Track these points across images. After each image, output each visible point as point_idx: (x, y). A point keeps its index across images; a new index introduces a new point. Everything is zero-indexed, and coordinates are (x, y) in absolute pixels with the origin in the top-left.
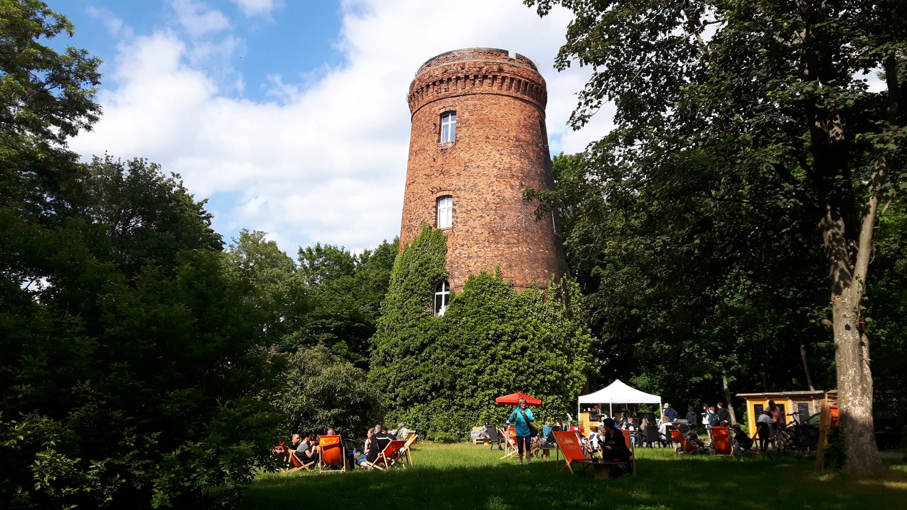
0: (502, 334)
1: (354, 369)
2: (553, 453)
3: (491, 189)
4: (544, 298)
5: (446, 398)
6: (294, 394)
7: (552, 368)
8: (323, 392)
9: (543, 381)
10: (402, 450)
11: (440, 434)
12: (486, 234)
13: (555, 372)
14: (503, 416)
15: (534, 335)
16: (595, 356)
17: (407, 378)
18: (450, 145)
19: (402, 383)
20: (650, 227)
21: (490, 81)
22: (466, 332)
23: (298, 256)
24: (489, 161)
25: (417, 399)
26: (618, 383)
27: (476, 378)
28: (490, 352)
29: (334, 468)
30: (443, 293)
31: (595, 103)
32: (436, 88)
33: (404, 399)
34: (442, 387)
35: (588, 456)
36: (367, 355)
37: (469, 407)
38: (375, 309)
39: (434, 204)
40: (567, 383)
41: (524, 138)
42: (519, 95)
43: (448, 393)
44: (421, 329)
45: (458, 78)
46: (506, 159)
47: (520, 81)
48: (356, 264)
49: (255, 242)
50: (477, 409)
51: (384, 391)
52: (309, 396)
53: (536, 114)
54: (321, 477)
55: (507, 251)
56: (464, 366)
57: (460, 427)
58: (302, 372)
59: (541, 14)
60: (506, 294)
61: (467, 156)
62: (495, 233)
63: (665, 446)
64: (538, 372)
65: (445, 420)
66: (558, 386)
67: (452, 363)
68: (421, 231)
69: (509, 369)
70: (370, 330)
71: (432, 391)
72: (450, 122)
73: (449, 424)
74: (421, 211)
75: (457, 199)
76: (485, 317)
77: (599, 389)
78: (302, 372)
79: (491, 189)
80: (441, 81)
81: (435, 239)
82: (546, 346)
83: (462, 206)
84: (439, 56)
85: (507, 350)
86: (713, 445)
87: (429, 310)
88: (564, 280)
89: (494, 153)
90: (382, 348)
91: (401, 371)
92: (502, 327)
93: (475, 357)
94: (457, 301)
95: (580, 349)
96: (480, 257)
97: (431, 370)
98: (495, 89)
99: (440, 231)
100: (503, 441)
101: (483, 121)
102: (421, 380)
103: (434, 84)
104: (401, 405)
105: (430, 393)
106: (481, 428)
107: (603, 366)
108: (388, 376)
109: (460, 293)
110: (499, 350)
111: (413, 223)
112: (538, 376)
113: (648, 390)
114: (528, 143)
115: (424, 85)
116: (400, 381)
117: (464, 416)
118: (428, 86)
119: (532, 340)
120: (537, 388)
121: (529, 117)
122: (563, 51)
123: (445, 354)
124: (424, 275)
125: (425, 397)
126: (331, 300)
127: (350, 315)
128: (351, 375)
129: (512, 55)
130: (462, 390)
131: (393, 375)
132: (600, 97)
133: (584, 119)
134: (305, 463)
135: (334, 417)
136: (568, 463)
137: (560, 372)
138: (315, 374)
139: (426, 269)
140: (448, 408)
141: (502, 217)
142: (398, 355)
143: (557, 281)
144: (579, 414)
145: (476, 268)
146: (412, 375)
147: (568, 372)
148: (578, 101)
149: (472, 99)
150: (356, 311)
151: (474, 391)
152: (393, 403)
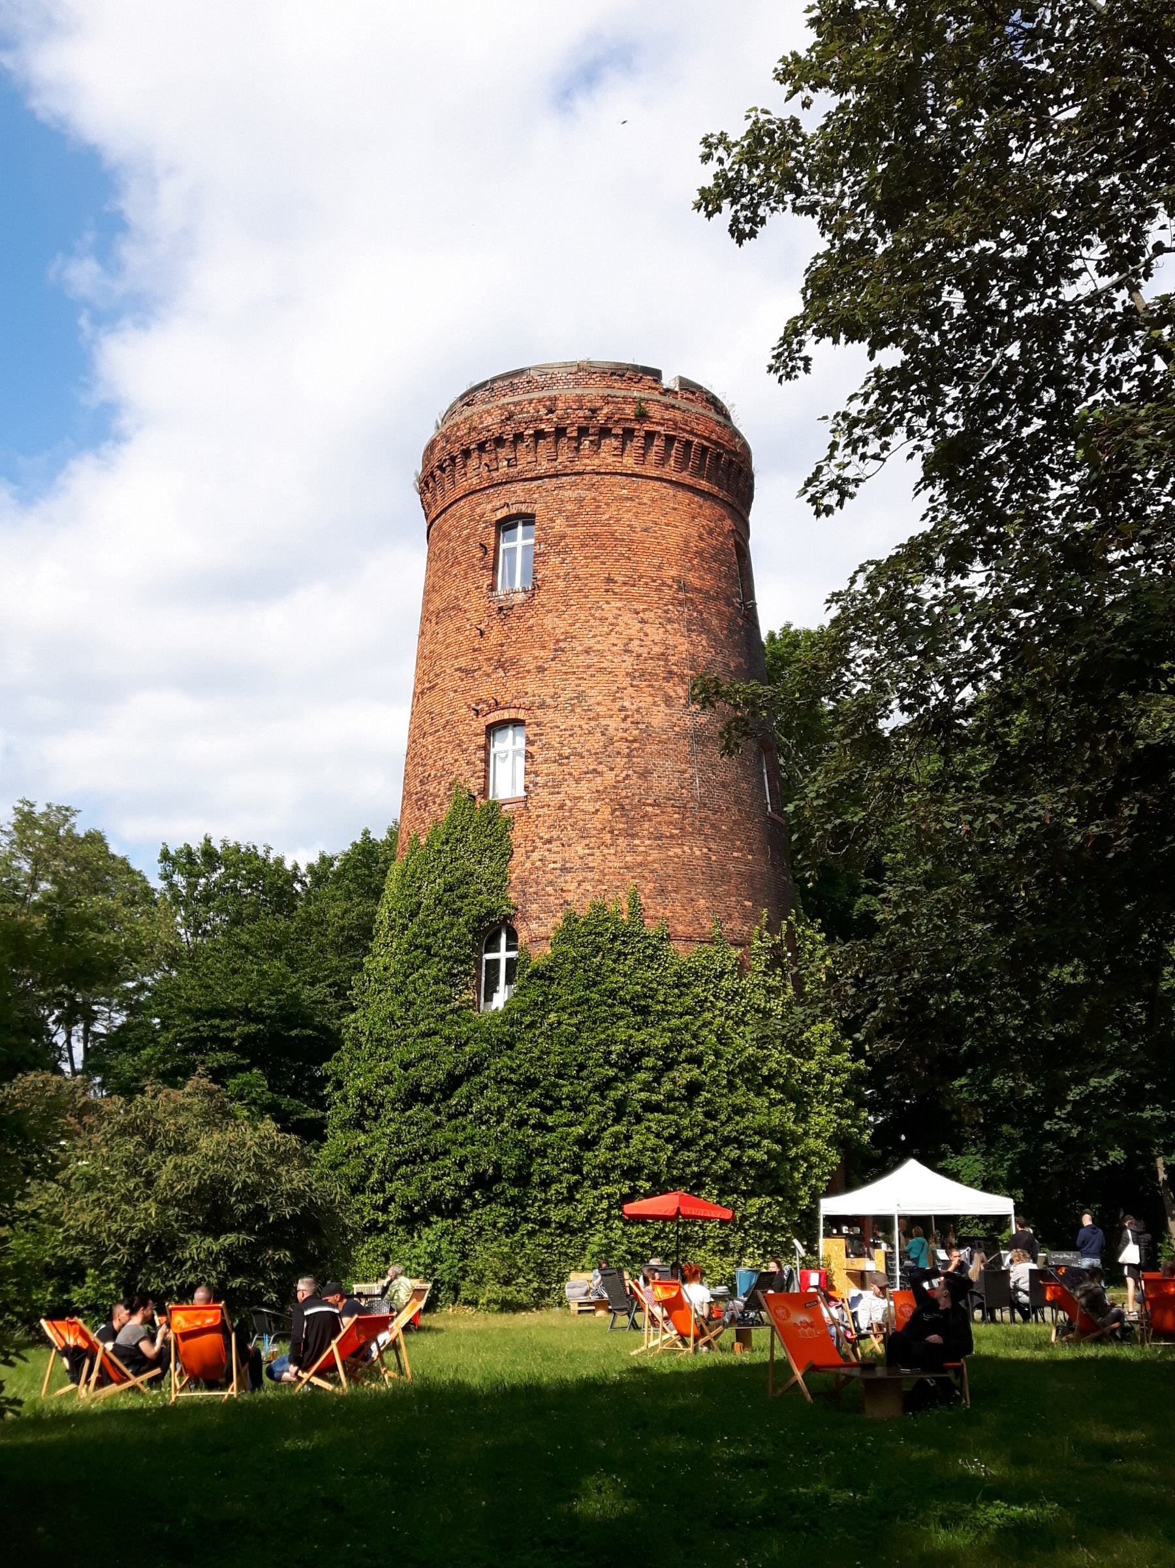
0: (643, 1054)
1: (278, 1138)
2: (760, 1336)
3: (618, 705)
4: (741, 968)
5: (507, 1205)
6: (128, 1199)
7: (760, 1132)
8: (199, 1190)
9: (737, 1164)
10: (384, 1337)
11: (492, 1290)
12: (606, 813)
13: (765, 1142)
14: (643, 1245)
15: (718, 1055)
16: (861, 1103)
17: (414, 1158)
18: (521, 597)
19: (403, 1170)
20: (1012, 775)
21: (615, 443)
22: (557, 1048)
23: (159, 868)
24: (613, 638)
25: (437, 1206)
26: (912, 1169)
27: (578, 1157)
28: (612, 1093)
29: (211, 1386)
30: (503, 955)
31: (874, 447)
32: (486, 458)
33: (409, 1208)
34: (497, 1178)
35: (846, 1348)
36: (321, 1103)
37: (561, 1225)
38: (340, 995)
39: (482, 740)
40: (795, 1168)
41: (697, 583)
42: (686, 477)
43: (514, 1191)
44: (448, 1041)
45: (539, 435)
46: (655, 633)
47: (688, 444)
48: (298, 887)
49: (51, 832)
50: (581, 1230)
51: (356, 1190)
52: (164, 1203)
53: (728, 524)
54: (167, 1412)
55: (655, 855)
56: (551, 1130)
57: (540, 1274)
58: (151, 1145)
59: (740, 236)
60: (651, 958)
61: (562, 625)
62: (627, 814)
63: (1026, 1317)
64: (727, 1141)
65: (504, 1257)
66: (772, 1175)
67: (521, 1123)
68: (448, 806)
69: (658, 1136)
70: (327, 1043)
71: (473, 1188)
72: (520, 541)
73: (515, 1265)
74: (449, 758)
75: (537, 730)
76: (603, 1011)
77: (864, 1182)
78: (151, 1145)
79: (618, 705)
80: (499, 442)
81: (482, 827)
82: (746, 1081)
83: (547, 747)
84: (494, 380)
85: (652, 1091)
86: (1147, 1318)
87: (469, 995)
88: (790, 924)
89: (627, 617)
90: (356, 1084)
91: (400, 1142)
92: (641, 1036)
93: (576, 1108)
94: (537, 974)
95: (826, 1088)
96: (591, 869)
97: (471, 1140)
98: (629, 461)
99: (495, 806)
100: (640, 1309)
101: (599, 540)
102: (448, 1162)
103: (481, 447)
104: (399, 1222)
105: (469, 1193)
106: (589, 1276)
107: (877, 1128)
108: (368, 1152)
109: (542, 954)
110: (634, 1089)
111: (431, 787)
112: (726, 1151)
113: (988, 1186)
114: (708, 597)
115: (456, 450)
116: (397, 1165)
117: (549, 1247)
118: (466, 453)
119: (713, 1066)
120: (723, 1178)
121: (710, 532)
122: (794, 330)
123: (504, 1100)
124: (456, 913)
125: (457, 1202)
126: (235, 971)
127: (281, 1008)
128: (272, 1153)
129: (668, 381)
130: (545, 1184)
131: (379, 1152)
132: (886, 431)
133: (843, 488)
134: (136, 1374)
135: (227, 1253)
136: (798, 1375)
137: (778, 1142)
138: (181, 1148)
139: (463, 897)
140: (511, 1228)
141: (644, 774)
142: (393, 1102)
143: (772, 927)
144: (822, 1240)
145: (580, 895)
146: (426, 1152)
147: (797, 1140)
148: (830, 439)
149: (574, 485)
150: (295, 997)
151: (573, 1188)
152: (382, 1218)
